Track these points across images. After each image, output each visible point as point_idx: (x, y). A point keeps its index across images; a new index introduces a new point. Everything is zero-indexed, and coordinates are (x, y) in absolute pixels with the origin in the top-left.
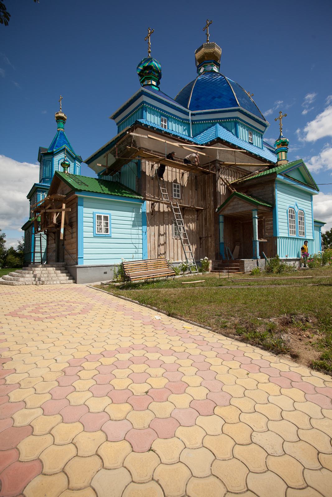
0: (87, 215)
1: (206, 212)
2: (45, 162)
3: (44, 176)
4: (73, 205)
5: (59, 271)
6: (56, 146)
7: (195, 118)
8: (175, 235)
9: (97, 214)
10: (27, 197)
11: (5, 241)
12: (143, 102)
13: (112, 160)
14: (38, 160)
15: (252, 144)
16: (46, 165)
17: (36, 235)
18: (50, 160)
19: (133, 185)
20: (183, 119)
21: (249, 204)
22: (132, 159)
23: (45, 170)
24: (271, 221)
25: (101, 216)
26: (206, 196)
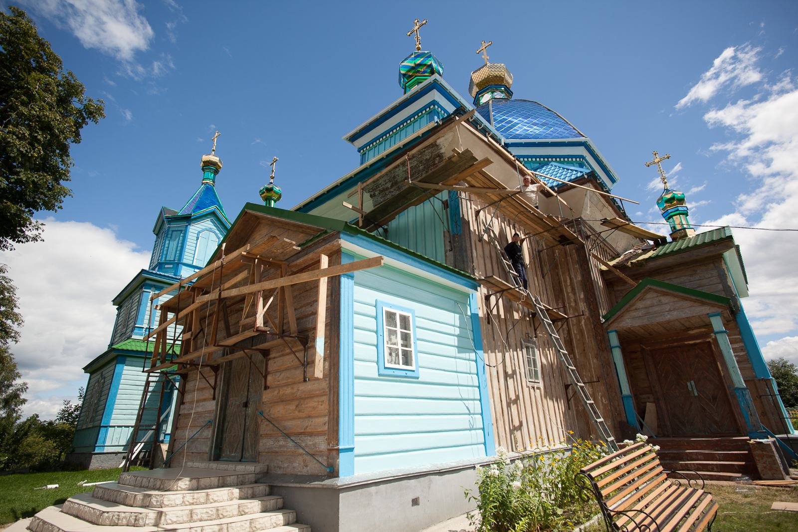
1: (568, 325)
2: (170, 232)
3: (163, 259)
5: (255, 505)
8: (531, 378)
9: (386, 309)
10: (113, 301)
11: (24, 401)
12: (434, 103)
14: (154, 231)
16: (171, 238)
17: (151, 374)
18: (181, 231)
21: (695, 301)
22: (443, 187)
23: (168, 247)
24: (737, 343)
25: (395, 314)
26: (561, 291)
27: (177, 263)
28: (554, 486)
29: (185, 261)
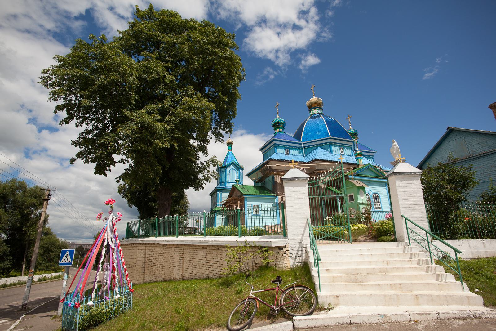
0: (249, 205)
4: (243, 201)
6: (228, 162)
7: (305, 145)
13: (260, 175)
15: (344, 154)
19: (271, 188)
20: (299, 147)
27: (225, 182)
28: (477, 277)
29: (227, 181)
